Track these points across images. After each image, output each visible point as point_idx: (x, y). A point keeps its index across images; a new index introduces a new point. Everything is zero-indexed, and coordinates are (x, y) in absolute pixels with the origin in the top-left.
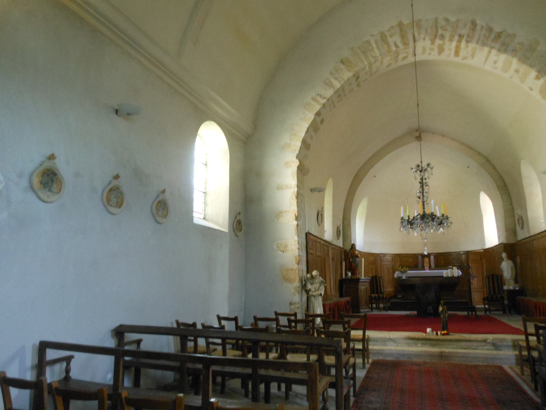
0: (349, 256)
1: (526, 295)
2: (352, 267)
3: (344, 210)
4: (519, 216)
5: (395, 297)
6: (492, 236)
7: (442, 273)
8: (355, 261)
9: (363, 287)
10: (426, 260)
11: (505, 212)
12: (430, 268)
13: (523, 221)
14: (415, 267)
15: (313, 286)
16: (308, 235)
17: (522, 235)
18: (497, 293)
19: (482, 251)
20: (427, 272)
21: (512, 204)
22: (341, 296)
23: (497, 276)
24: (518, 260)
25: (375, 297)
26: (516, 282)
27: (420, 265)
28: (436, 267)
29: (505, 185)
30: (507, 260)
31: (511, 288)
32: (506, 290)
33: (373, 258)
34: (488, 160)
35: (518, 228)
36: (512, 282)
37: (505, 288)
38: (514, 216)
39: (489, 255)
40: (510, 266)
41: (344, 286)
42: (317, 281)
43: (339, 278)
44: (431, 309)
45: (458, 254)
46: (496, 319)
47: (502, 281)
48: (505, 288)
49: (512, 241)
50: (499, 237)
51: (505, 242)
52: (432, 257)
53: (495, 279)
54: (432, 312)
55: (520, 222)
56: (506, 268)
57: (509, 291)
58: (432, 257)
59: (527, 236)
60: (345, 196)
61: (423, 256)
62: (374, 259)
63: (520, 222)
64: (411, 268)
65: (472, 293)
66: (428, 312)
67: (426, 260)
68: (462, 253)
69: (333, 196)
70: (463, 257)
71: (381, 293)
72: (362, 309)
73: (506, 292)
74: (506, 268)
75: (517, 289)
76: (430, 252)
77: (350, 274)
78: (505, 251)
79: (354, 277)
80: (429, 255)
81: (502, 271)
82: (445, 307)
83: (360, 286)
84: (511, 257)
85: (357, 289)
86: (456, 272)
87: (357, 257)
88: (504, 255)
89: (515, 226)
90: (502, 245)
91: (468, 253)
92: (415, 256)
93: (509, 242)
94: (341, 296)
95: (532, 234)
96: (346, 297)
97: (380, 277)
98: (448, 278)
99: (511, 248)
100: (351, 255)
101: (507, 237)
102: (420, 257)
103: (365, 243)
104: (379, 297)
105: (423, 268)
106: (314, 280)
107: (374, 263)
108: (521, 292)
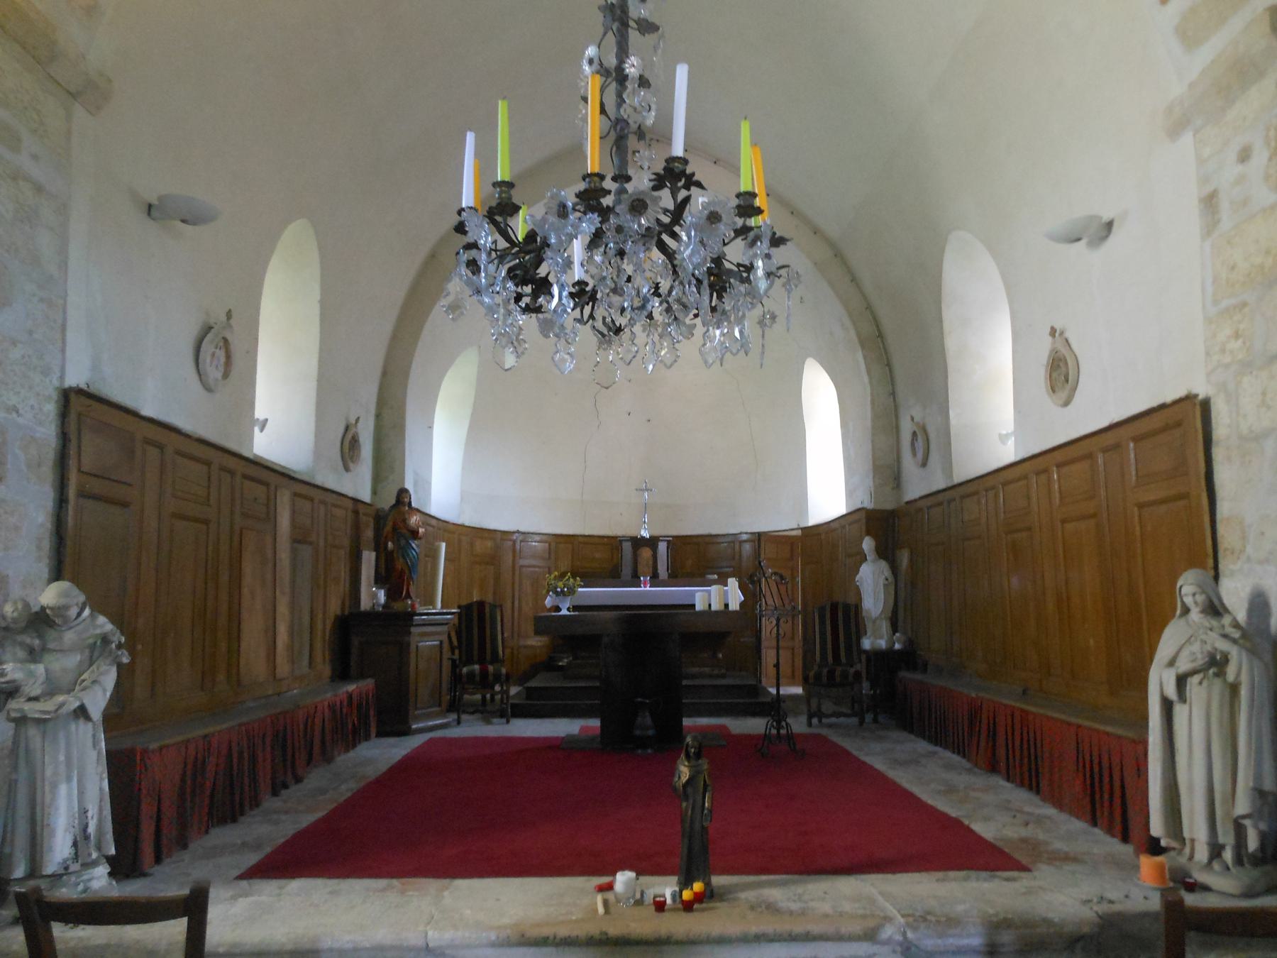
0: (392, 528)
1: (925, 669)
2: (394, 576)
3: (385, 373)
4: (918, 424)
5: (548, 665)
6: (827, 489)
7: (693, 594)
8: (404, 550)
9: (426, 643)
10: (646, 553)
11: (876, 417)
12: (655, 579)
13: (930, 441)
14: (612, 575)
15: (40, 669)
16: (73, 397)
17: (919, 483)
18: (843, 660)
19: (799, 533)
20: (645, 592)
21: (893, 394)
22: (342, 672)
23: (847, 607)
24: (904, 558)
25: (471, 675)
26: (894, 627)
27: (627, 571)
28: (670, 576)
29: (881, 335)
30: (873, 561)
31: (882, 644)
32: (866, 652)
33: (489, 544)
34: (838, 254)
35: (909, 464)
36: (885, 627)
37: (867, 644)
38: (897, 428)
39: (817, 541)
40: (882, 581)
41: (356, 641)
42: (69, 637)
43: (334, 607)
44: (649, 721)
45: (734, 539)
46: (848, 753)
47: (857, 625)
48: (867, 644)
49: (889, 506)
50: (850, 493)
51: (869, 505)
52: (662, 547)
53: (843, 616)
54: (651, 732)
55: (920, 443)
56: (871, 584)
57: (878, 657)
58: (662, 547)
59: (940, 484)
60: (388, 328)
61: (638, 542)
62: (484, 549)
63: (920, 443)
64: (590, 578)
65: (764, 651)
66: (638, 732)
67: (646, 553)
68: (745, 537)
69: (323, 303)
70: (747, 548)
71: (495, 659)
72: (418, 719)
73: (864, 657)
74: (871, 584)
75: (897, 646)
76: (657, 533)
77: (382, 596)
78: (868, 533)
79: (397, 606)
80: (652, 542)
81: (859, 594)
82: (704, 764)
83: (414, 640)
84: (885, 552)
85: (403, 648)
86: (732, 595)
87: (414, 534)
88: (868, 544)
89: (898, 460)
90: (863, 515)
91: (759, 538)
92: (613, 543)
93: (879, 507)
94: (342, 672)
95: (961, 474)
96: (362, 676)
97: (494, 607)
98: (708, 613)
99: (884, 525)
100: (395, 529)
101: (877, 492)
102: (627, 547)
103: (464, 497)
104: (484, 672)
105: (635, 580)
106: (51, 634)
107: (493, 559)
108: (908, 658)
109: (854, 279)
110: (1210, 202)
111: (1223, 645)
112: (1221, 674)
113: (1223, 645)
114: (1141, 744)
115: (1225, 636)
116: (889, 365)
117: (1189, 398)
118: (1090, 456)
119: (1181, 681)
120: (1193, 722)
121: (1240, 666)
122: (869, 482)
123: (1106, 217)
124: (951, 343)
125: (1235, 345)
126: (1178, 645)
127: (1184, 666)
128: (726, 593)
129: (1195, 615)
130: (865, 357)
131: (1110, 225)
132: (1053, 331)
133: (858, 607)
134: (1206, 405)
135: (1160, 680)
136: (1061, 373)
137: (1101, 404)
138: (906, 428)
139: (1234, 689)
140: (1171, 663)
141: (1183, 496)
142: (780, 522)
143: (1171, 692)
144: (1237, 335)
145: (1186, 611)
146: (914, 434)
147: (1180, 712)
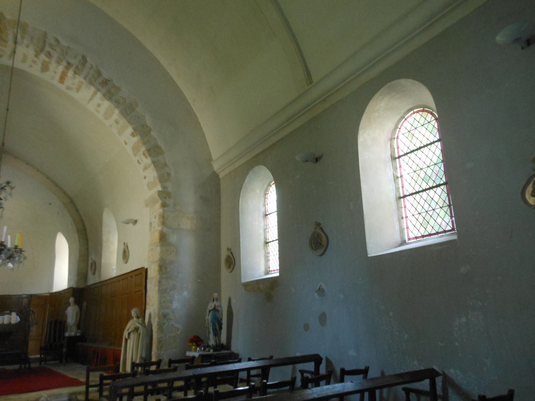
13: (95, 267)
17: (92, 280)
21: (87, 249)
24: (85, 304)
31: (73, 334)
32: (67, 337)
34: (72, 202)
35: (90, 273)
36: (75, 328)
37: (67, 334)
38: (88, 260)
45: (20, 297)
48: (67, 334)
49: (82, 286)
51: (74, 286)
53: (59, 324)
55: (93, 267)
56: (71, 313)
57: (70, 338)
59: (97, 280)
63: (93, 267)
68: (25, 296)
74: (71, 313)
75: (78, 334)
78: (73, 296)
84: (78, 302)
86: (14, 318)
88: (72, 300)
89: (87, 272)
91: (31, 297)
95: (102, 279)
101: (78, 282)
109: (77, 210)
110: (151, 224)
111: (138, 325)
112: (137, 331)
113: (138, 325)
114: (120, 351)
115: (139, 323)
116: (87, 239)
117: (143, 268)
118: (127, 278)
119: (129, 334)
120: (130, 343)
121: (141, 330)
122: (76, 278)
123: (135, 219)
124: (104, 238)
125: (151, 257)
126: (131, 325)
127: (130, 330)
128: (10, 318)
129: (135, 319)
130: (78, 236)
131: (136, 221)
132: (124, 243)
133: (65, 322)
134: (146, 270)
135: (126, 334)
136: (125, 255)
137: (132, 265)
138: (90, 262)
139: (140, 334)
140: (128, 330)
141: (141, 290)
142: (40, 290)
143: (127, 337)
144: (152, 255)
145: (133, 318)
146: (92, 264)
147: (129, 341)
